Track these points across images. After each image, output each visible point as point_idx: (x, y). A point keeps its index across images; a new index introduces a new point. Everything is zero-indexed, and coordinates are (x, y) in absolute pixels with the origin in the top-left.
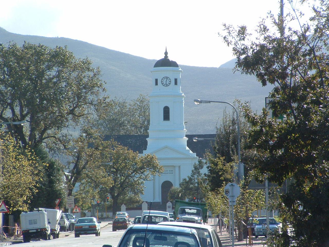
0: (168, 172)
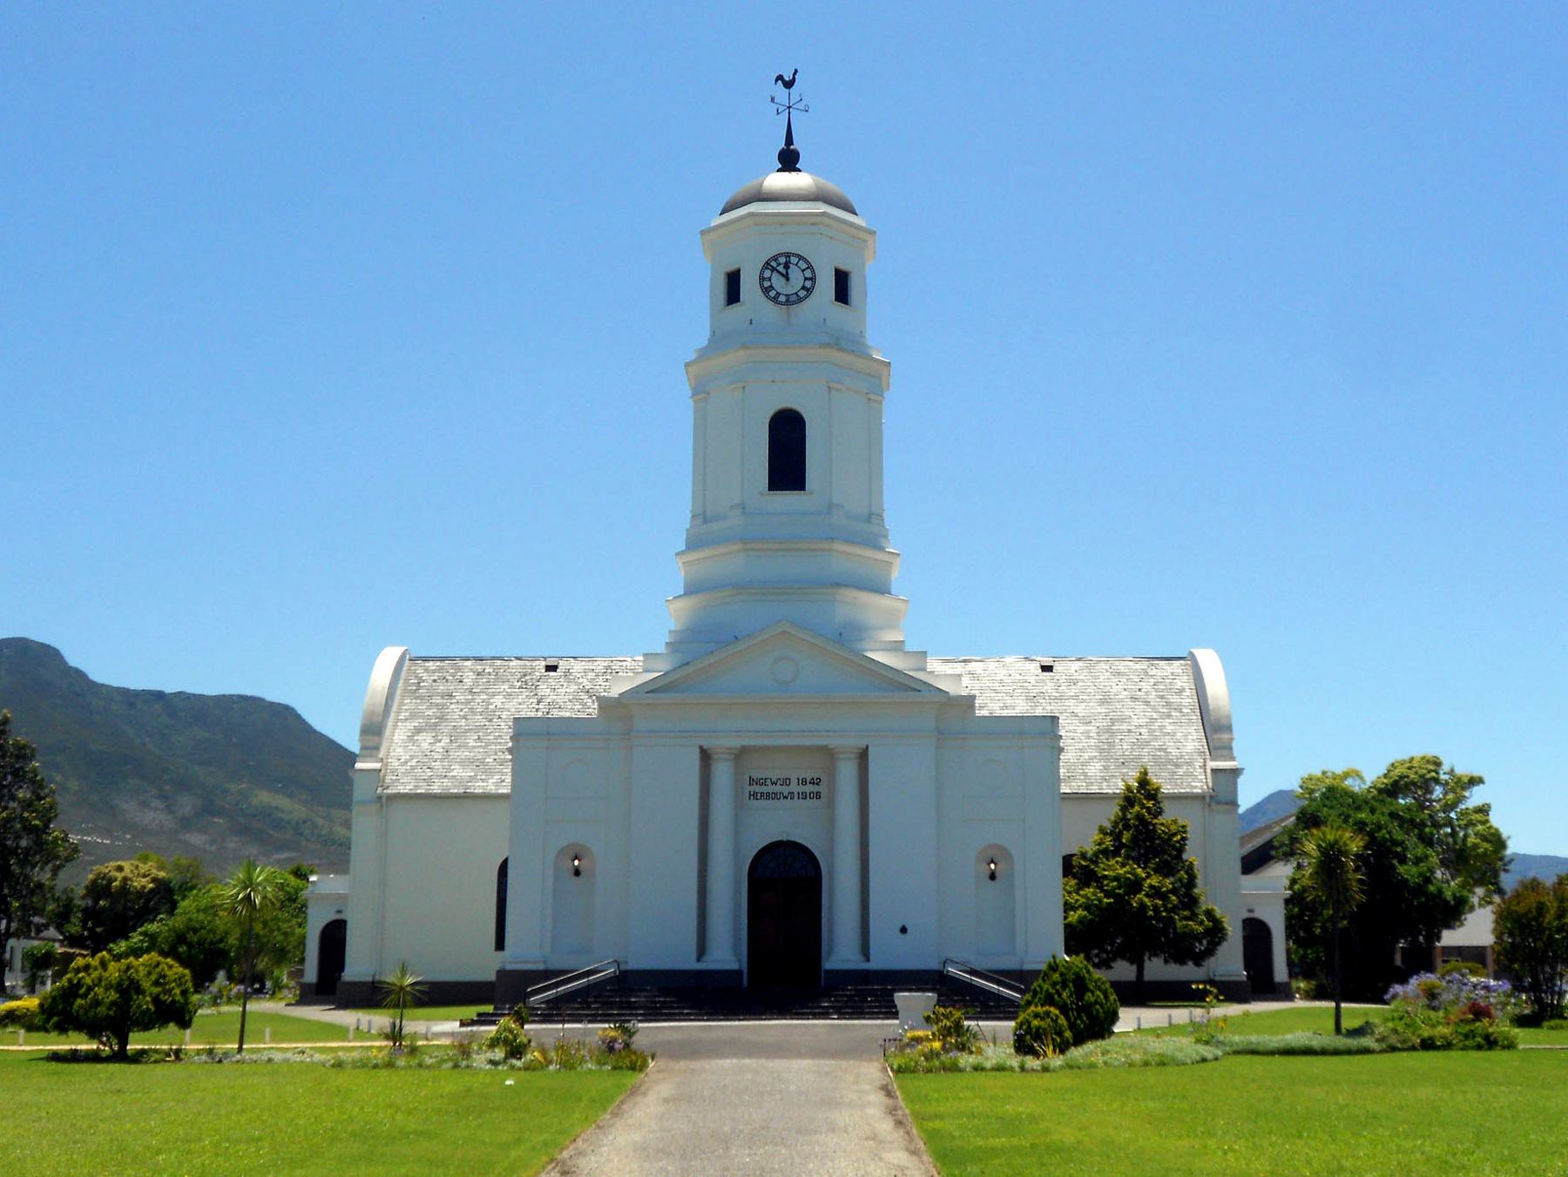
0: (795, 788)
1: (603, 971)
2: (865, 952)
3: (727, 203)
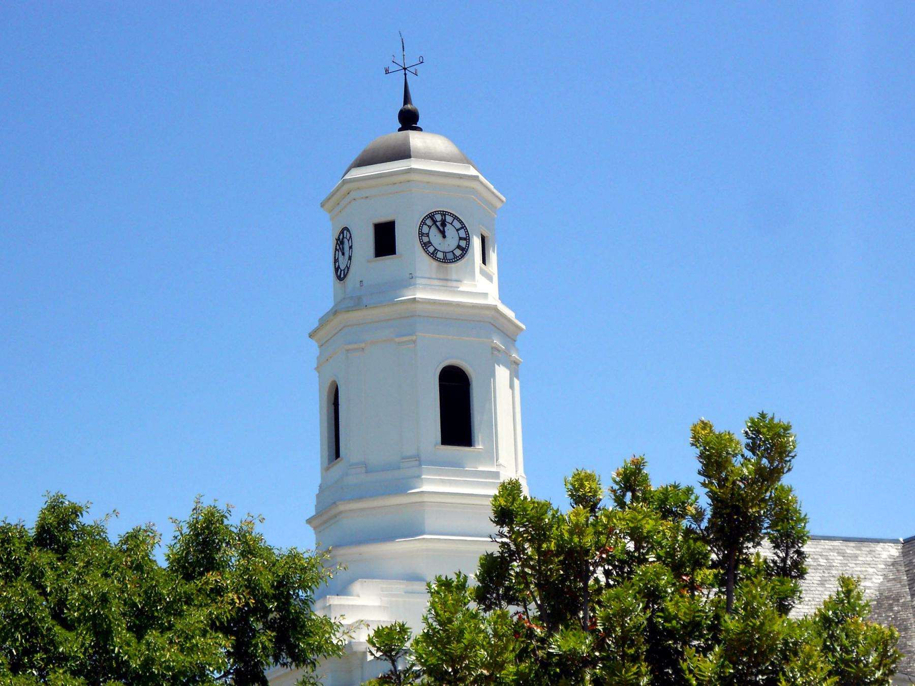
3: (365, 151)
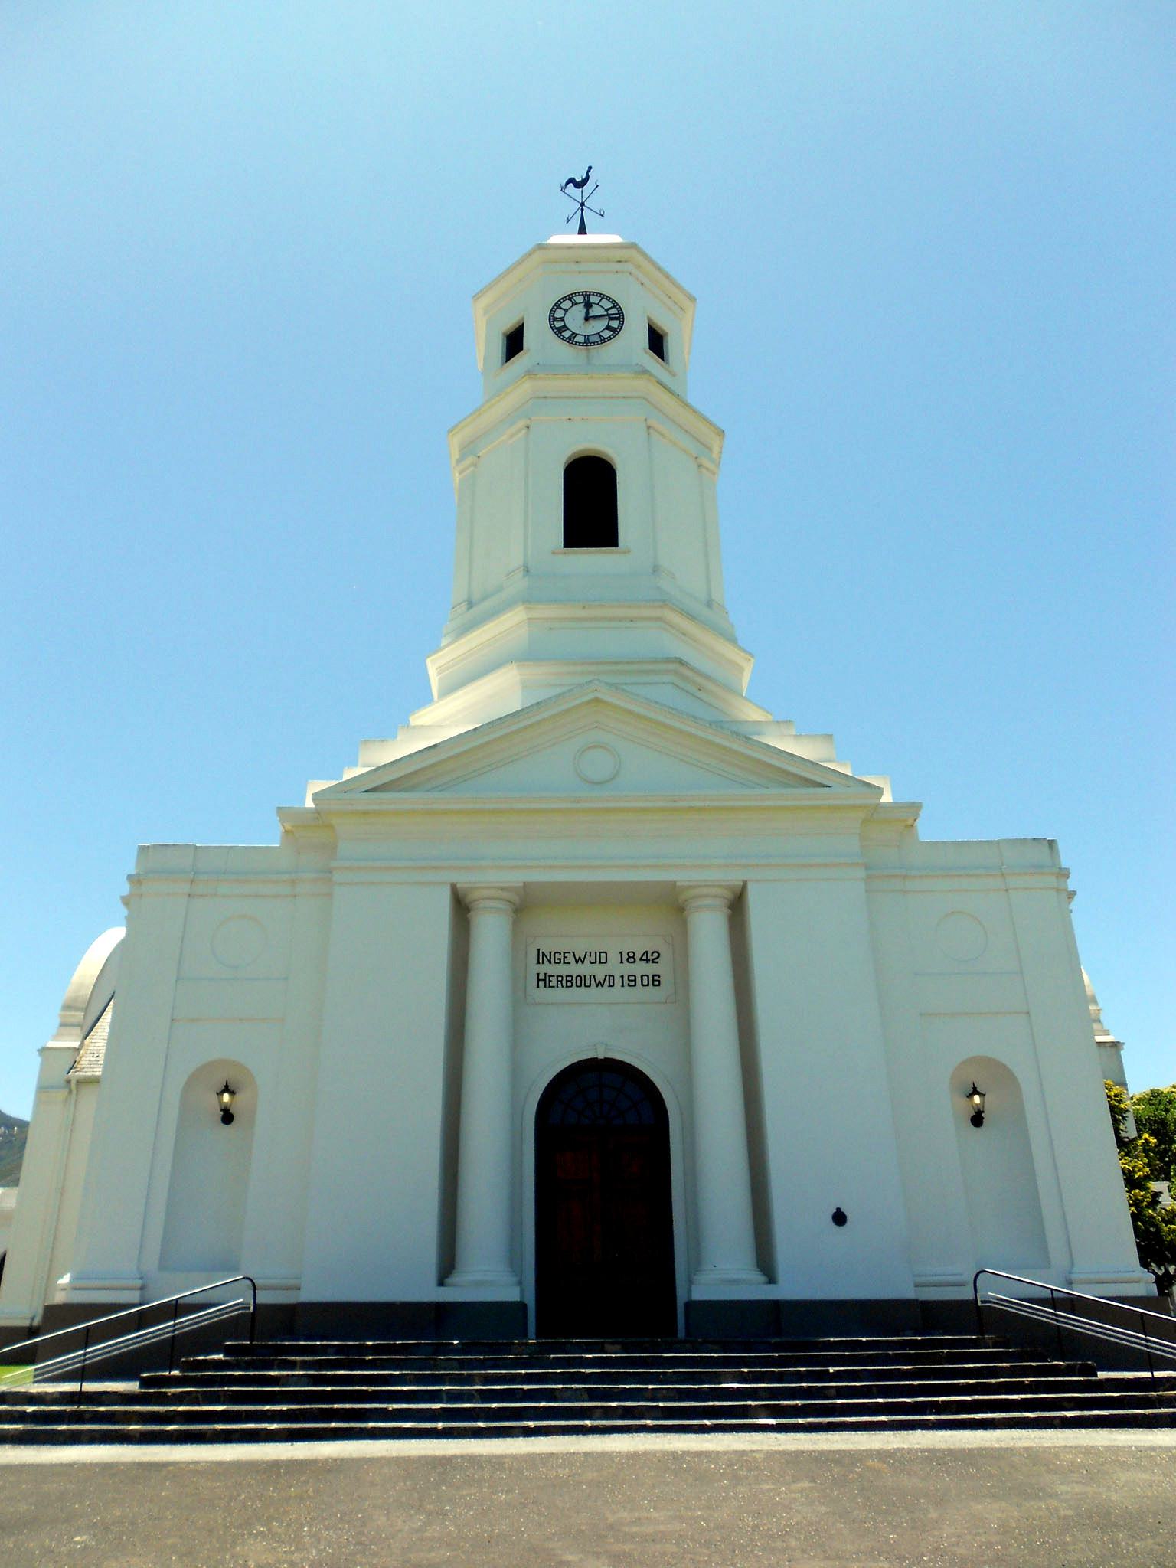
0: (616, 968)
1: (222, 1305)
2: (765, 1263)
